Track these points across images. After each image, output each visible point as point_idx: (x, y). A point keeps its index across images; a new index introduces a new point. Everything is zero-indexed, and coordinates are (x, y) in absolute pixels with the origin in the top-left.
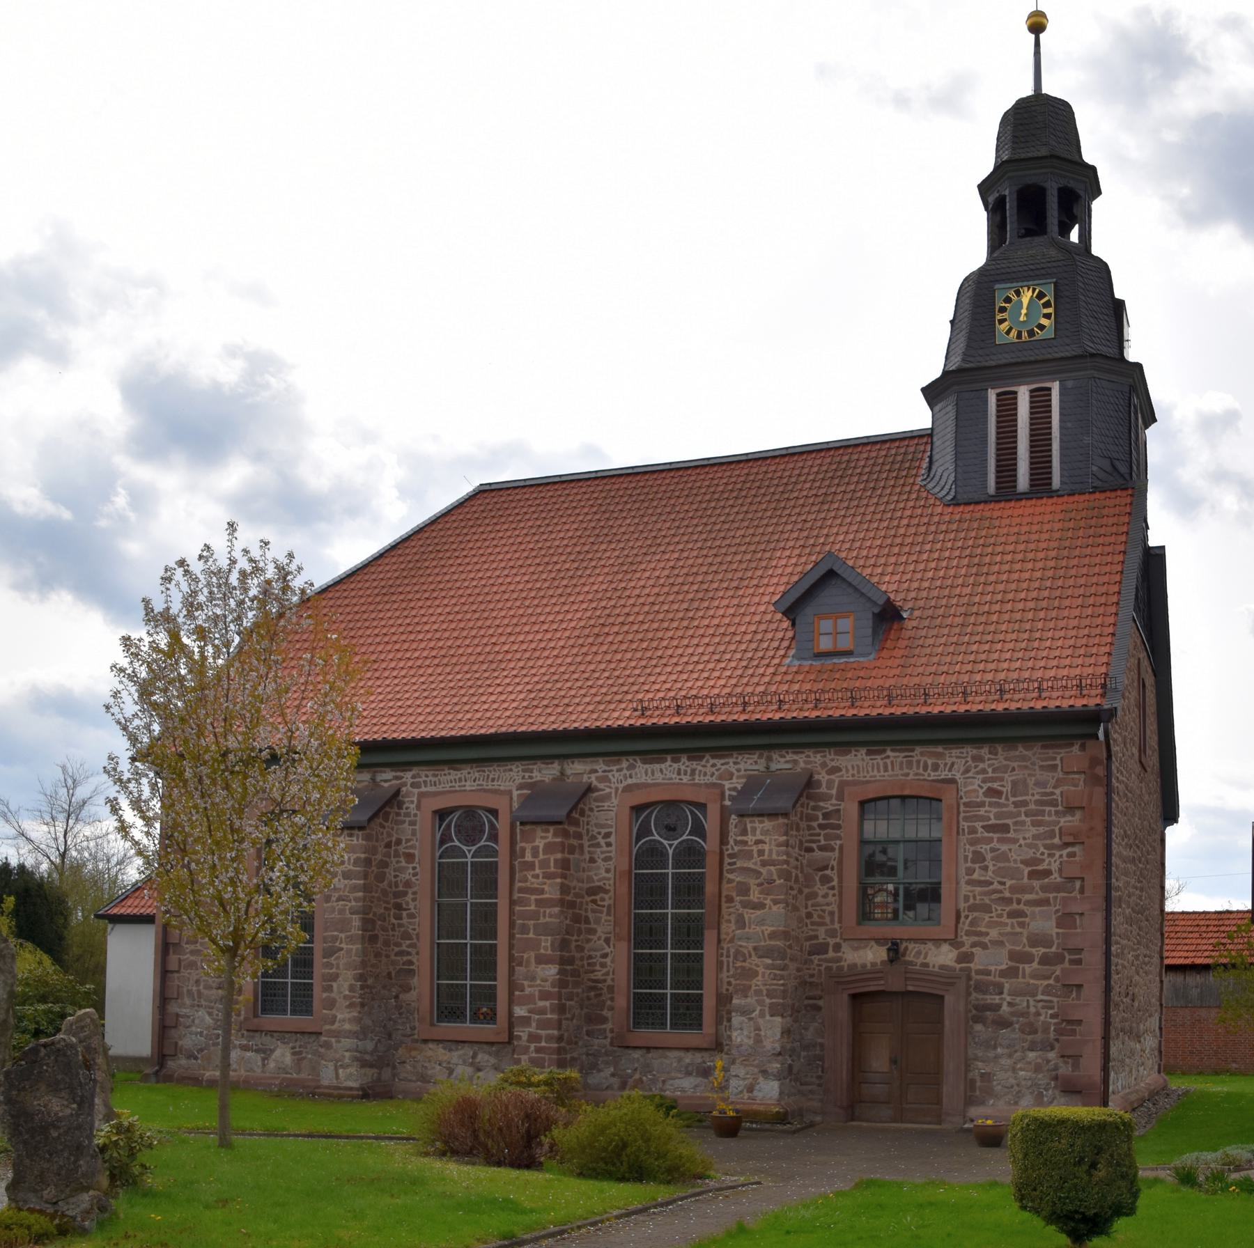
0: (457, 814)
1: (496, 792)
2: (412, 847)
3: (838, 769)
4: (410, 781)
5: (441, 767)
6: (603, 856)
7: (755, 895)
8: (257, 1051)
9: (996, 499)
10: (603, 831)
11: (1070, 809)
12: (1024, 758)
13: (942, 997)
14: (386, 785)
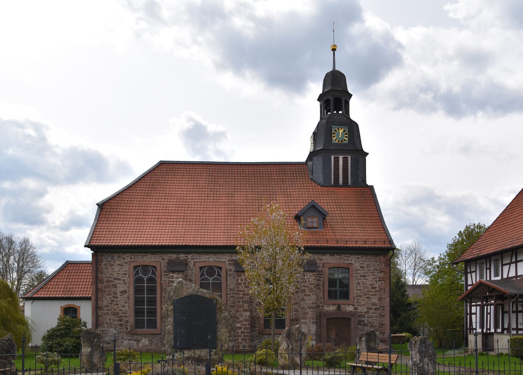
2: (192, 277)
3: (322, 260)
4: (190, 258)
7: (307, 293)
9: (332, 186)
11: (381, 272)
12: (370, 259)
13: (350, 319)
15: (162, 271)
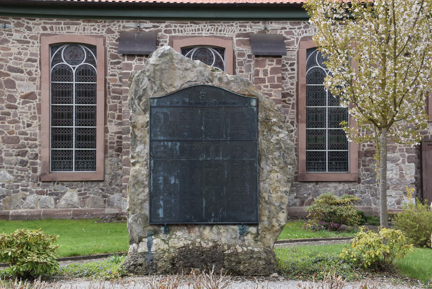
0: (195, 50)
1: (222, 38)
4: (164, 29)
5: (186, 22)
6: (289, 76)
8: (50, 194)
10: (290, 62)
14: (147, 30)
15: (108, 54)
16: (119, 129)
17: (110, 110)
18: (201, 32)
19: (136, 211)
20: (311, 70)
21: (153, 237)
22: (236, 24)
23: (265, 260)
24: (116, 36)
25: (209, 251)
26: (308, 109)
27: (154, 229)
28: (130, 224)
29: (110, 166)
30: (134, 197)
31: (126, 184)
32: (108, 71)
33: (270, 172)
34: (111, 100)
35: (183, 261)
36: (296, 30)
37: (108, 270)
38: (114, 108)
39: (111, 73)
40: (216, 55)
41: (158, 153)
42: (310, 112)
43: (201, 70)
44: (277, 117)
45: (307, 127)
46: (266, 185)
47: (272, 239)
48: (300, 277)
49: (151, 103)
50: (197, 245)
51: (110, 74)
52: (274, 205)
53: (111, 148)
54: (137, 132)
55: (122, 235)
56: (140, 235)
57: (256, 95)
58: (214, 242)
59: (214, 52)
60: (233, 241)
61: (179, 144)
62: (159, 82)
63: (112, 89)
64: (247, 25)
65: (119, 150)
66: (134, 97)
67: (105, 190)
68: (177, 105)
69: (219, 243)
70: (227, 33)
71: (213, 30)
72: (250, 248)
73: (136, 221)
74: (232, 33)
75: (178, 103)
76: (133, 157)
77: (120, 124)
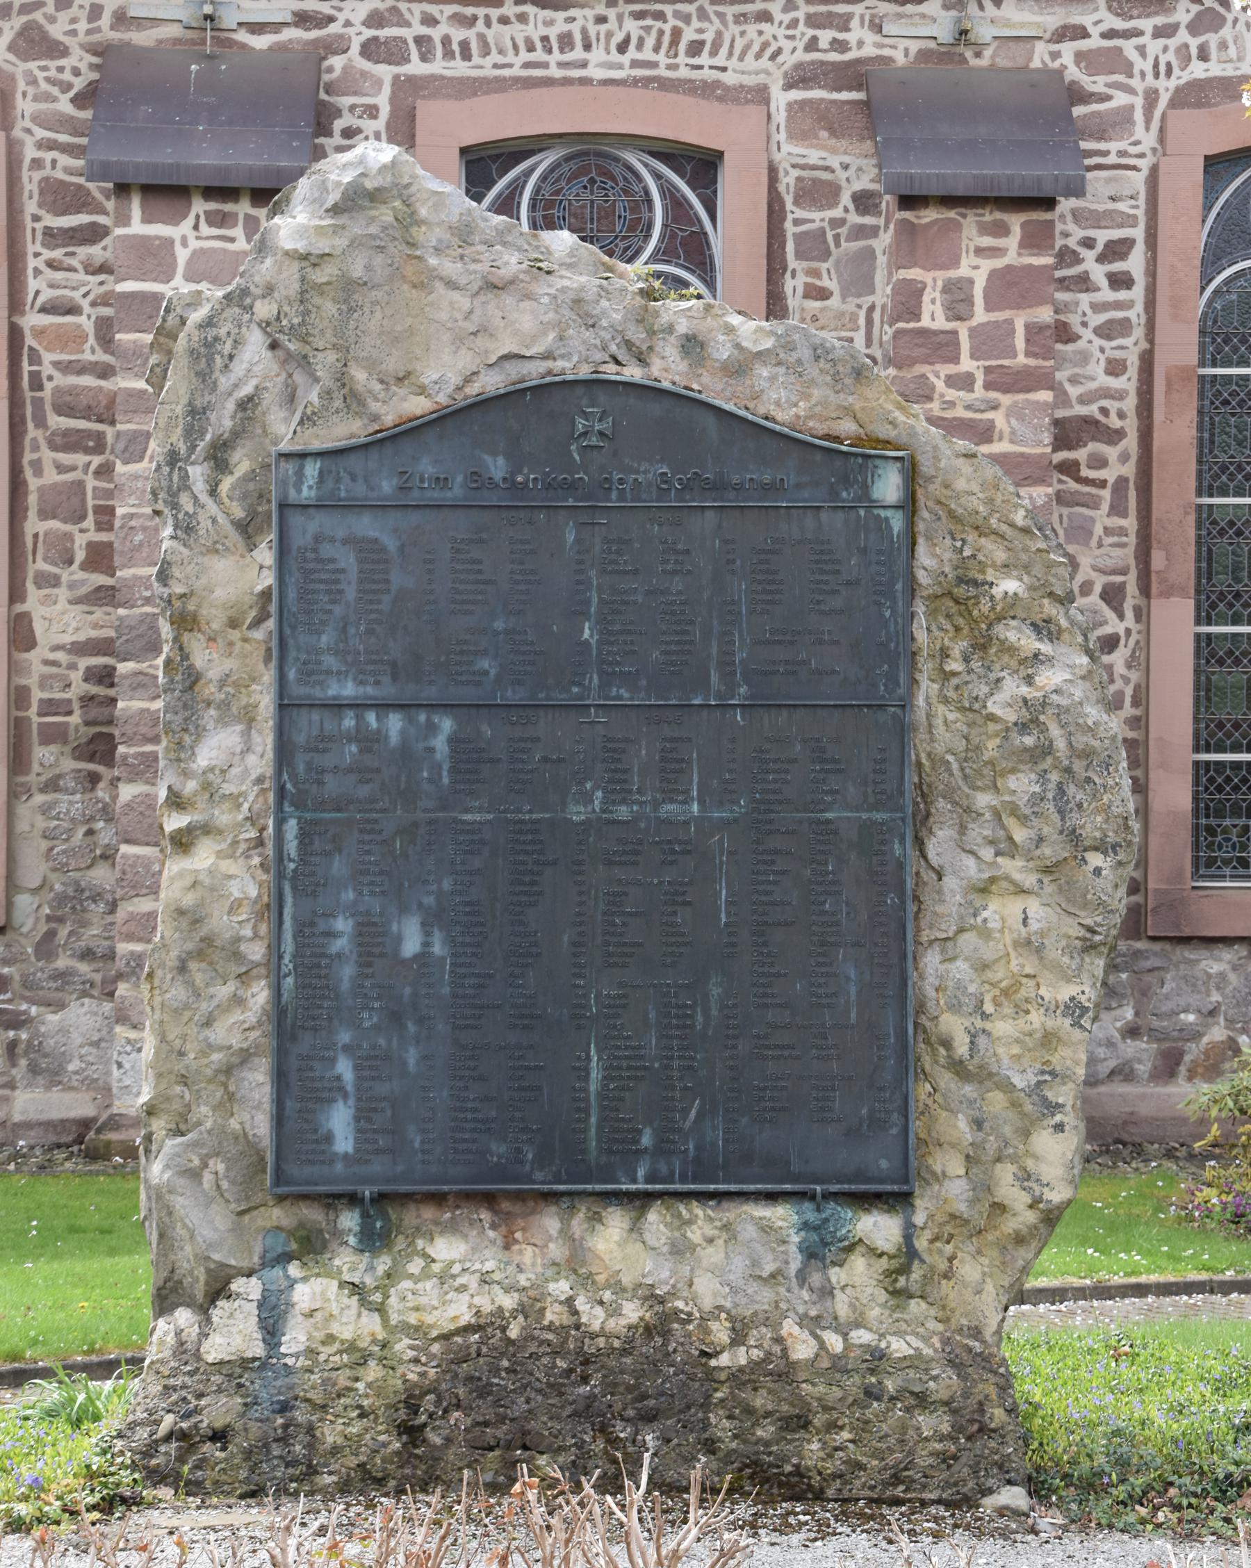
0: (546, 160)
1: (707, 90)
10: (1102, 237)
14: (260, 42)
15: (30, 182)
16: (96, 626)
17: (44, 515)
18: (578, 54)
19: (193, 1118)
20: (1227, 282)
21: (294, 1269)
22: (785, 10)
23: (954, 1412)
24: (76, 72)
25: (625, 1352)
26: (1205, 517)
27: (301, 1225)
28: (159, 1195)
29: (44, 845)
30: (184, 1037)
31: (138, 947)
32: (33, 284)
33: (984, 889)
34: (47, 455)
35: (467, 1410)
36: (1145, 39)
37: (24, 1469)
38: (67, 503)
39: (47, 295)
40: (676, 204)
41: (328, 778)
42: (1222, 532)
43: (582, 288)
44: (1026, 568)
45: (1198, 622)
46: (961, 969)
47: (990, 1287)
48: (1161, 1516)
49: (283, 483)
50: (549, 1317)
51: (41, 299)
52: (1007, 1086)
53: (52, 735)
54: (202, 655)
55: (112, 1252)
56: (216, 1256)
57: (904, 439)
58: (652, 1298)
59: (658, 176)
60: (764, 1297)
61: (447, 725)
62: (331, 357)
63: (57, 391)
64: (848, 17)
65: (99, 748)
66: (182, 448)
67: (16, 984)
68: (435, 495)
69: (680, 1304)
70: (733, 63)
71: (650, 42)
72: (862, 1336)
73: (194, 1175)
74: (764, 62)
75: (442, 482)
76: (176, 801)
77: (105, 596)
